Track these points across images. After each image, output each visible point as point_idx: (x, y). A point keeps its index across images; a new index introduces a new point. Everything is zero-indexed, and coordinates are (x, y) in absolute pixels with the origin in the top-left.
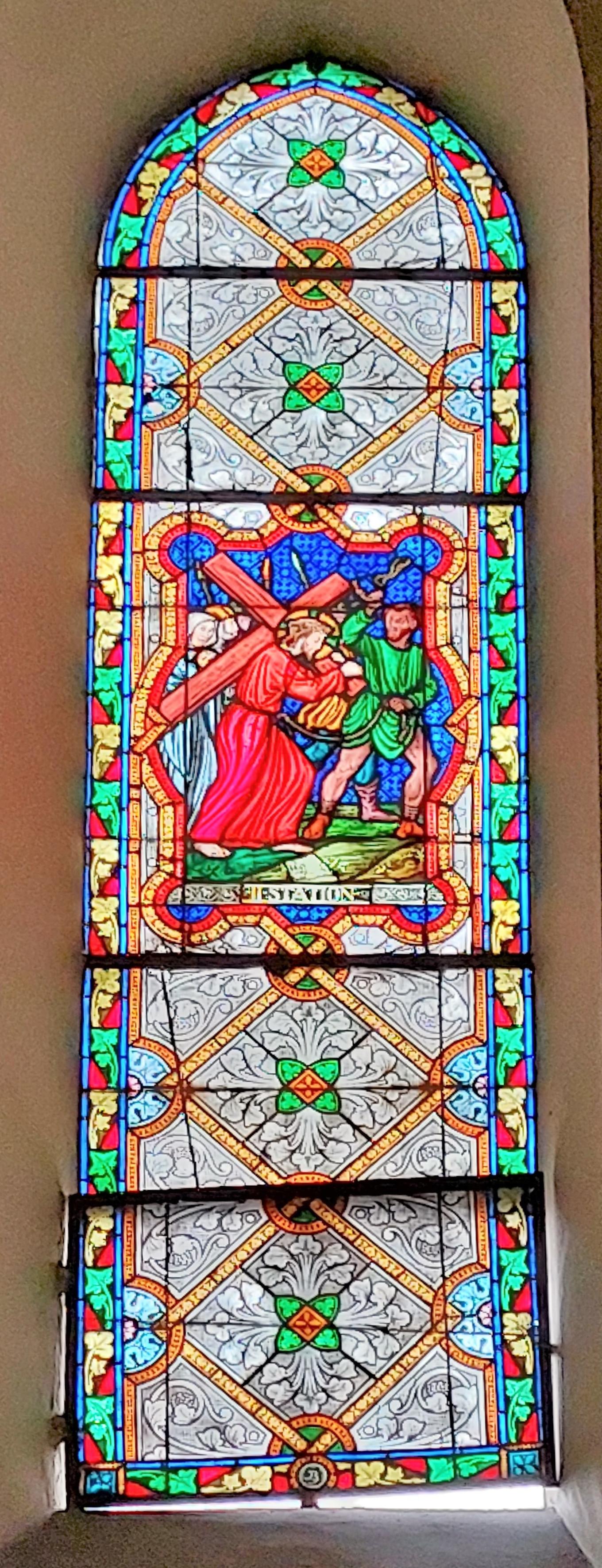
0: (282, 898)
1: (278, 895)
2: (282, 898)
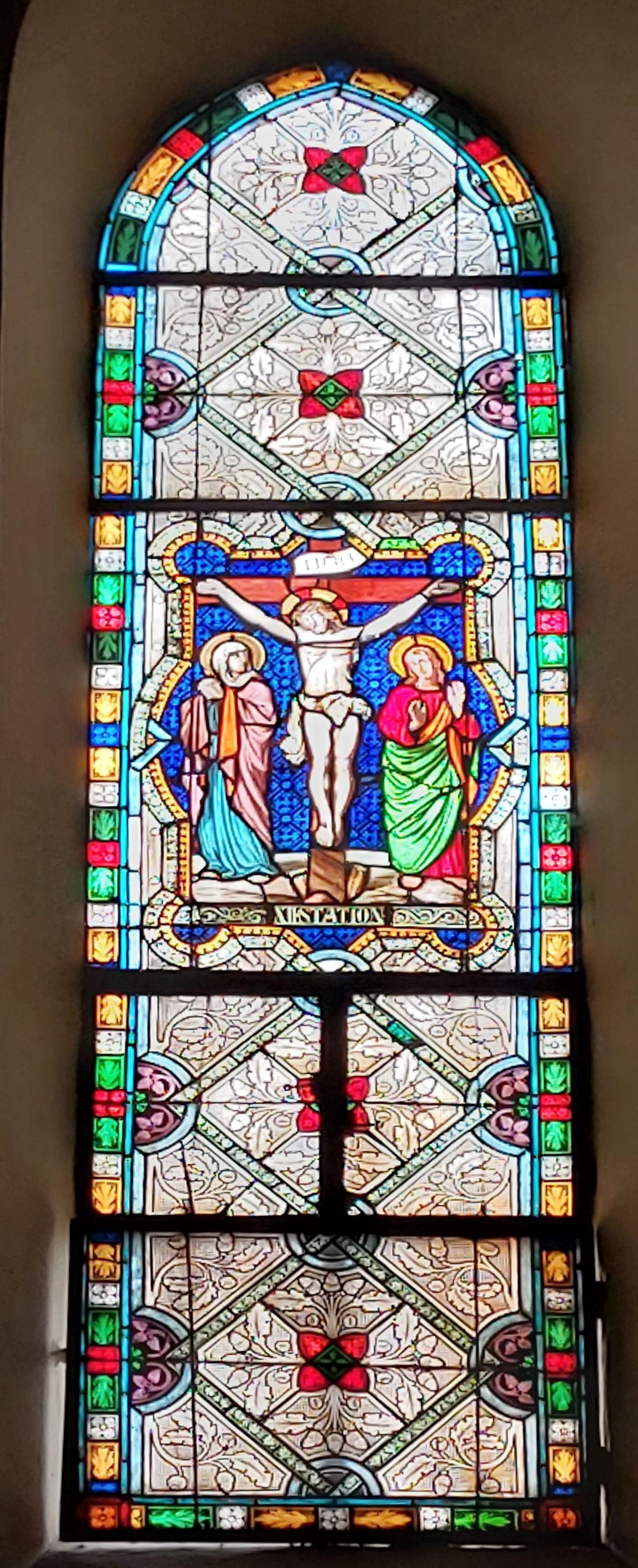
1: (308, 918)
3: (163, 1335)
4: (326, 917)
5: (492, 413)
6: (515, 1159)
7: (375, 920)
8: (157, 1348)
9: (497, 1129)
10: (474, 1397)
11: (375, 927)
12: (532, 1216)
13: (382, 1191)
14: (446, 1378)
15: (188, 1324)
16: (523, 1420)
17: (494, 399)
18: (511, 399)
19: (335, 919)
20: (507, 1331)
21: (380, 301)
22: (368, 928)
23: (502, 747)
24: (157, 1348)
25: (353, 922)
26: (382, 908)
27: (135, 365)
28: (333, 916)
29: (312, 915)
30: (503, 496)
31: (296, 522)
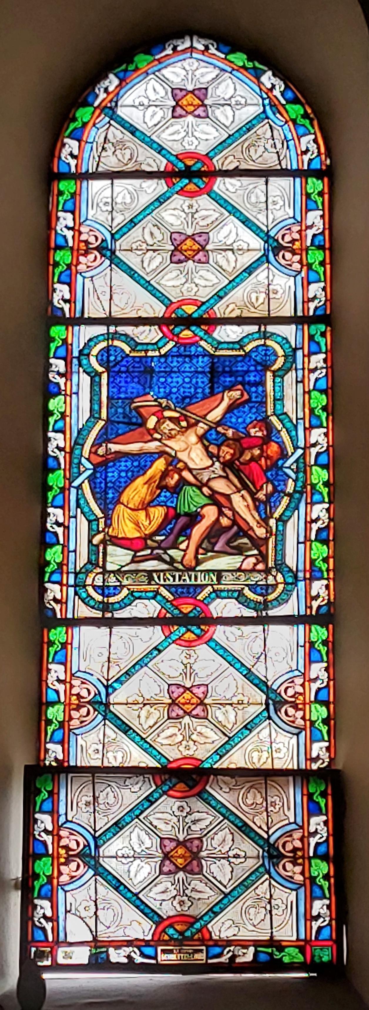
0: (174, 581)
1: (171, 579)
2: (174, 581)
3: (82, 700)
4: (183, 578)
5: (290, 717)
6: (293, 278)
7: (212, 581)
8: (75, 847)
9: (285, 716)
10: (267, 876)
11: (212, 585)
12: (306, 769)
13: (216, 151)
14: (251, 863)
15: (93, 832)
16: (297, 735)
17: (291, 707)
18: (300, 861)
19: (188, 580)
20: (288, 834)
21: (222, 187)
22: (207, 585)
23: (289, 468)
24: (75, 847)
25: (199, 582)
26: (216, 573)
27: (66, 814)
28: (187, 578)
29: (174, 577)
30: (293, 314)
31: (172, 132)
